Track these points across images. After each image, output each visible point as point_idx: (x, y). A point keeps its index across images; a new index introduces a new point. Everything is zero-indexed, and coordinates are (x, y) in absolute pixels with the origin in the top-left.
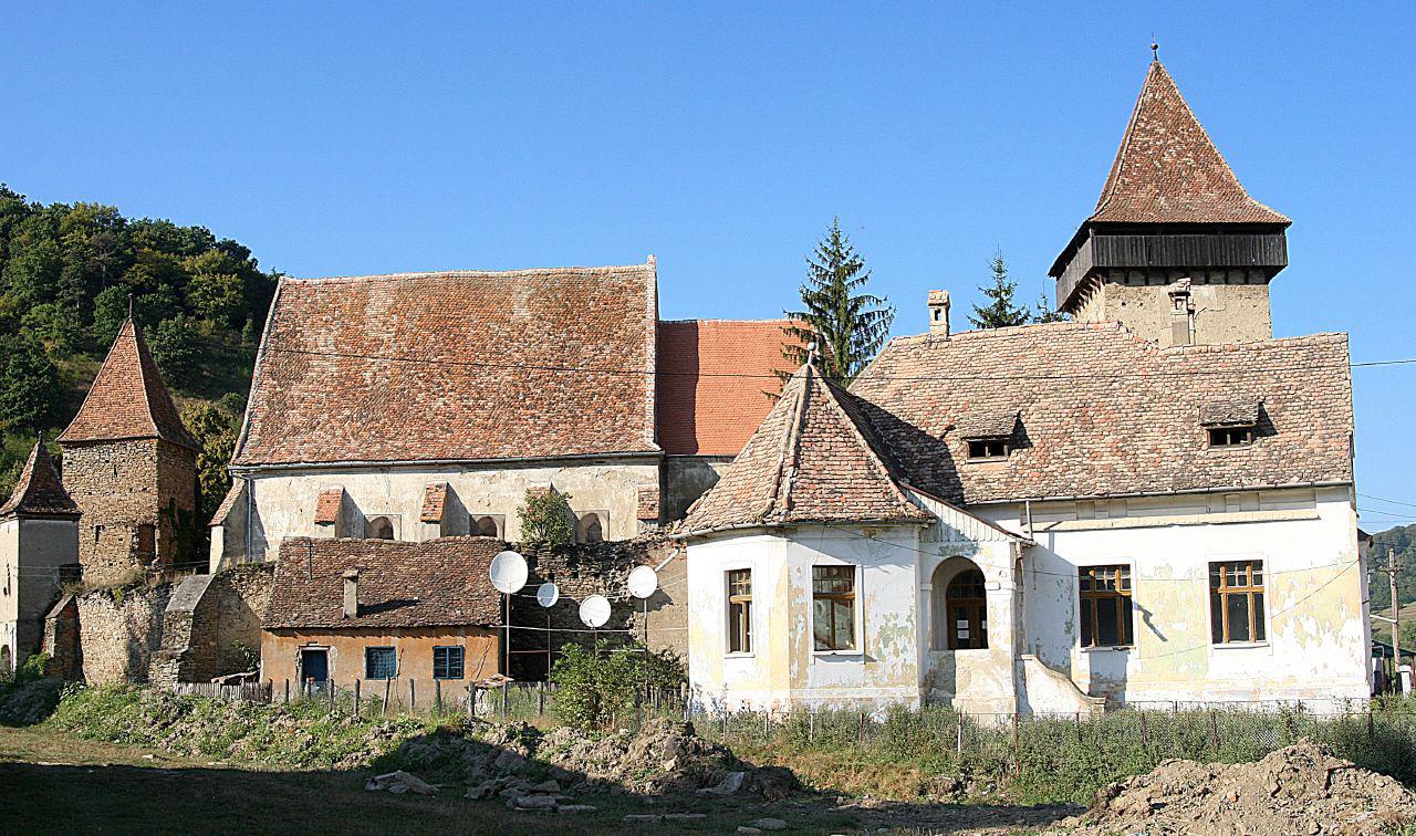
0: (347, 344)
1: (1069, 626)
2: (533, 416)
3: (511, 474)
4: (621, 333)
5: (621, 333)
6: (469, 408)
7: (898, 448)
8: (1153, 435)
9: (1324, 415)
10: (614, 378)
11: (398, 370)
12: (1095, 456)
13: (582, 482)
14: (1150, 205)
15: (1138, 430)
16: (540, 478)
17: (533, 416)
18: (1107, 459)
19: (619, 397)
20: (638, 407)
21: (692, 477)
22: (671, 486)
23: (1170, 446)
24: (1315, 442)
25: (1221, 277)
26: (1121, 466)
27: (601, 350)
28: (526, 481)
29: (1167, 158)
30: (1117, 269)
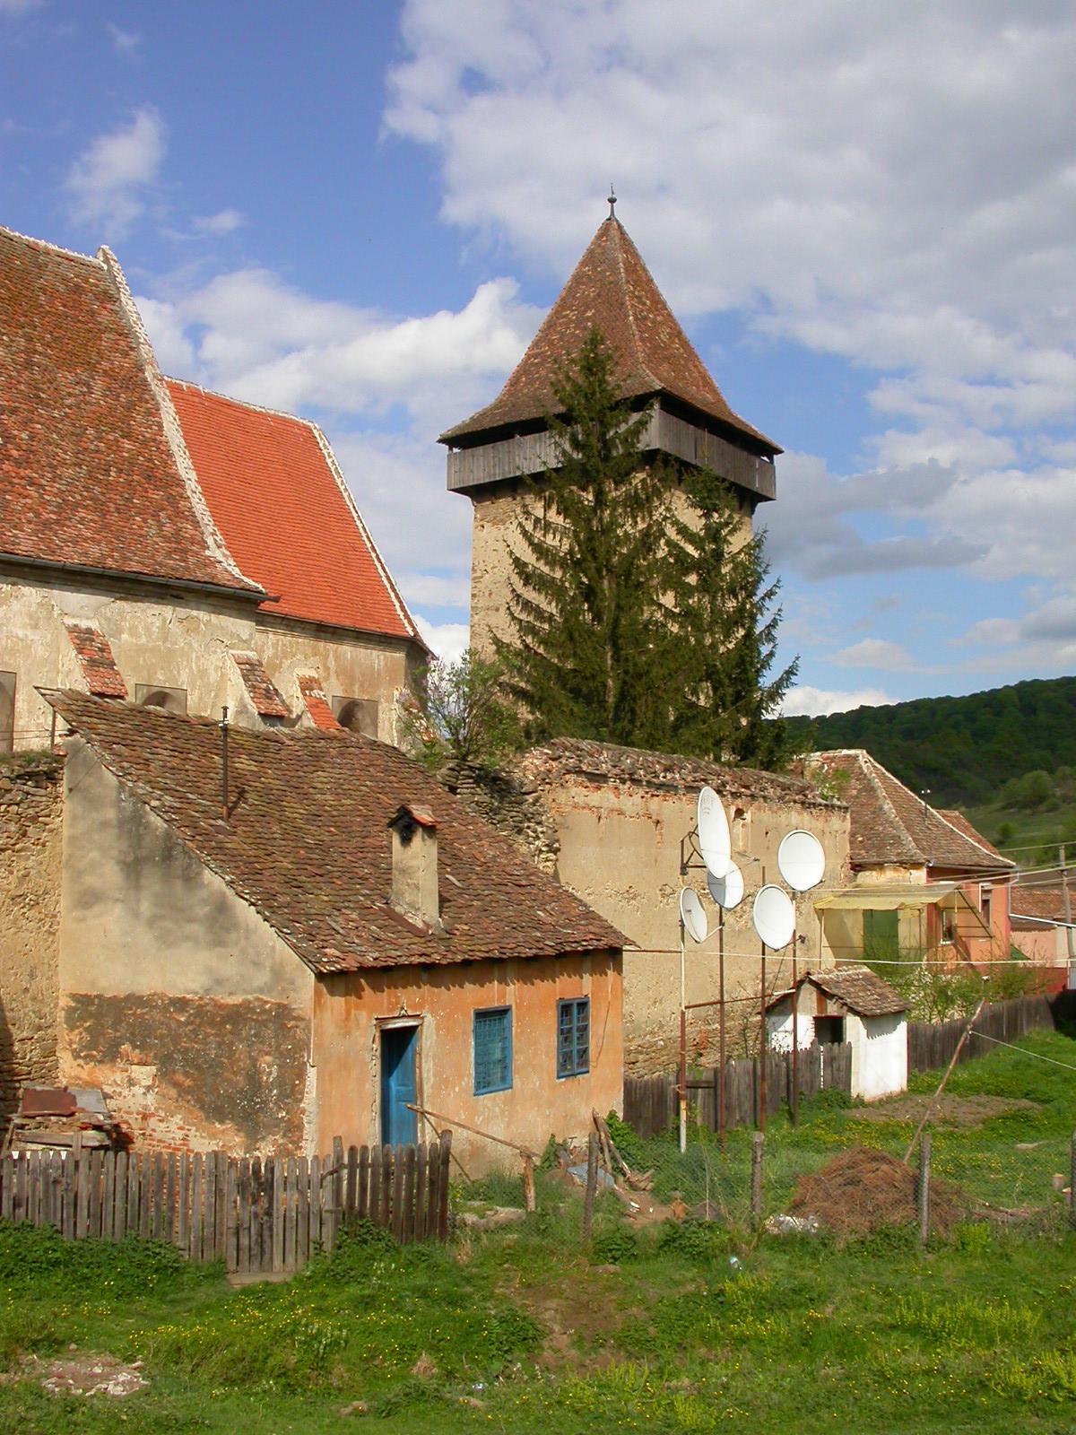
3: (32, 595)
10: (127, 444)
13: (148, 629)
16: (81, 607)
28: (57, 611)
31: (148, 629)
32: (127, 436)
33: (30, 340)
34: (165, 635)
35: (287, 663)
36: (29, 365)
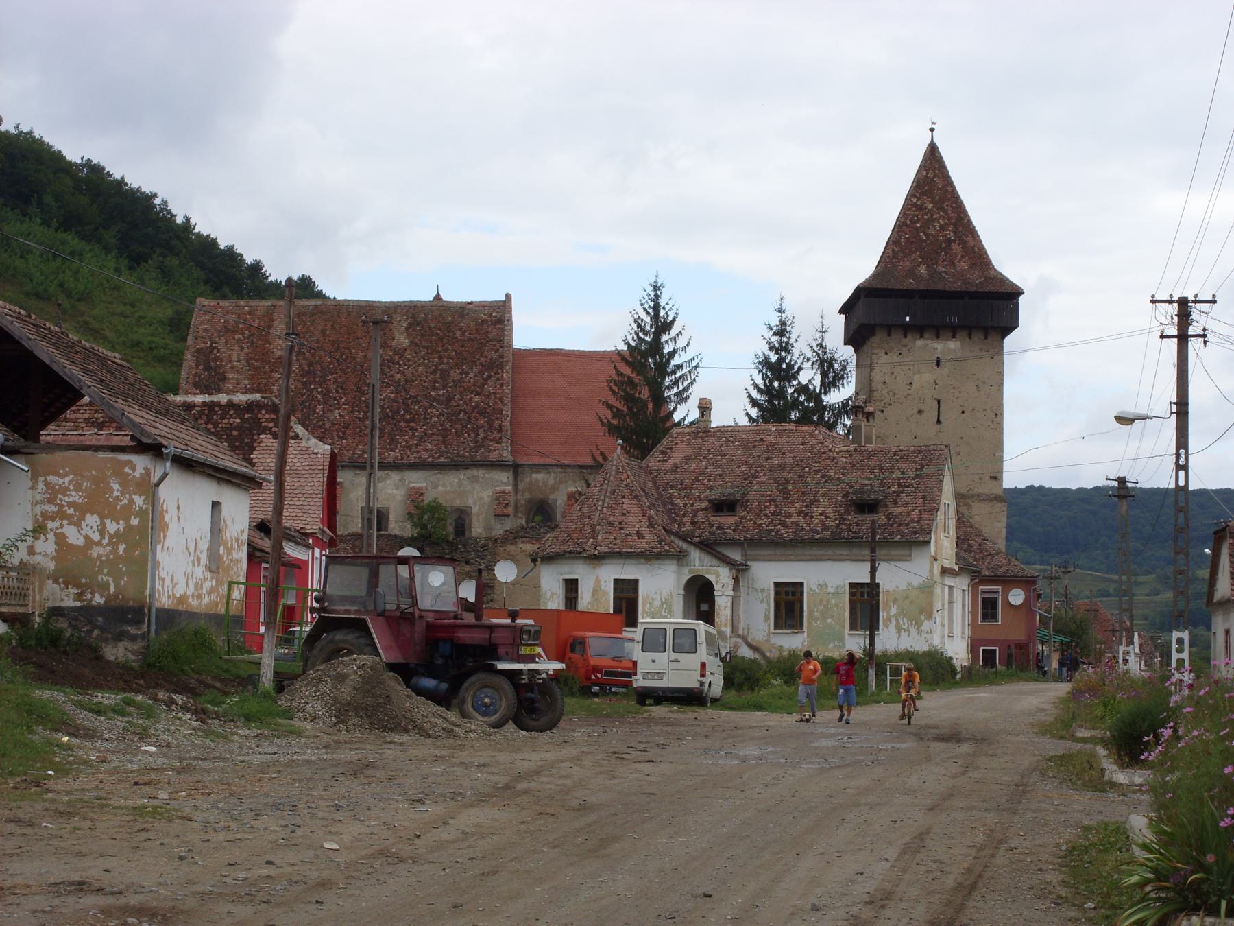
0: (257, 361)
1: (767, 618)
2: (412, 429)
4: (482, 360)
5: (482, 360)
6: (360, 419)
7: (672, 503)
8: (824, 503)
9: (924, 497)
10: (477, 399)
11: (300, 386)
12: (789, 516)
13: (451, 484)
14: (911, 273)
15: (815, 500)
16: (417, 479)
17: (412, 429)
18: (795, 518)
19: (480, 413)
20: (496, 424)
21: (537, 481)
22: (520, 487)
23: (827, 509)
24: (914, 515)
25: (965, 333)
26: (803, 524)
27: (467, 374)
29: (931, 231)
30: (881, 326)
31: (451, 484)
32: (478, 394)
33: (441, 358)
34: (460, 485)
35: (562, 486)
36: (434, 372)
